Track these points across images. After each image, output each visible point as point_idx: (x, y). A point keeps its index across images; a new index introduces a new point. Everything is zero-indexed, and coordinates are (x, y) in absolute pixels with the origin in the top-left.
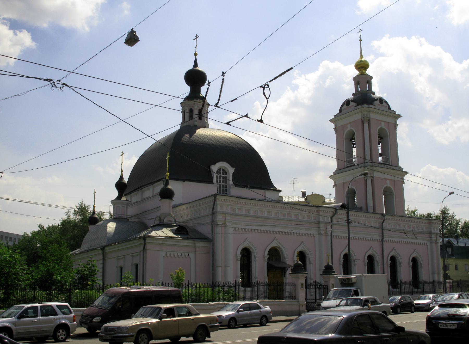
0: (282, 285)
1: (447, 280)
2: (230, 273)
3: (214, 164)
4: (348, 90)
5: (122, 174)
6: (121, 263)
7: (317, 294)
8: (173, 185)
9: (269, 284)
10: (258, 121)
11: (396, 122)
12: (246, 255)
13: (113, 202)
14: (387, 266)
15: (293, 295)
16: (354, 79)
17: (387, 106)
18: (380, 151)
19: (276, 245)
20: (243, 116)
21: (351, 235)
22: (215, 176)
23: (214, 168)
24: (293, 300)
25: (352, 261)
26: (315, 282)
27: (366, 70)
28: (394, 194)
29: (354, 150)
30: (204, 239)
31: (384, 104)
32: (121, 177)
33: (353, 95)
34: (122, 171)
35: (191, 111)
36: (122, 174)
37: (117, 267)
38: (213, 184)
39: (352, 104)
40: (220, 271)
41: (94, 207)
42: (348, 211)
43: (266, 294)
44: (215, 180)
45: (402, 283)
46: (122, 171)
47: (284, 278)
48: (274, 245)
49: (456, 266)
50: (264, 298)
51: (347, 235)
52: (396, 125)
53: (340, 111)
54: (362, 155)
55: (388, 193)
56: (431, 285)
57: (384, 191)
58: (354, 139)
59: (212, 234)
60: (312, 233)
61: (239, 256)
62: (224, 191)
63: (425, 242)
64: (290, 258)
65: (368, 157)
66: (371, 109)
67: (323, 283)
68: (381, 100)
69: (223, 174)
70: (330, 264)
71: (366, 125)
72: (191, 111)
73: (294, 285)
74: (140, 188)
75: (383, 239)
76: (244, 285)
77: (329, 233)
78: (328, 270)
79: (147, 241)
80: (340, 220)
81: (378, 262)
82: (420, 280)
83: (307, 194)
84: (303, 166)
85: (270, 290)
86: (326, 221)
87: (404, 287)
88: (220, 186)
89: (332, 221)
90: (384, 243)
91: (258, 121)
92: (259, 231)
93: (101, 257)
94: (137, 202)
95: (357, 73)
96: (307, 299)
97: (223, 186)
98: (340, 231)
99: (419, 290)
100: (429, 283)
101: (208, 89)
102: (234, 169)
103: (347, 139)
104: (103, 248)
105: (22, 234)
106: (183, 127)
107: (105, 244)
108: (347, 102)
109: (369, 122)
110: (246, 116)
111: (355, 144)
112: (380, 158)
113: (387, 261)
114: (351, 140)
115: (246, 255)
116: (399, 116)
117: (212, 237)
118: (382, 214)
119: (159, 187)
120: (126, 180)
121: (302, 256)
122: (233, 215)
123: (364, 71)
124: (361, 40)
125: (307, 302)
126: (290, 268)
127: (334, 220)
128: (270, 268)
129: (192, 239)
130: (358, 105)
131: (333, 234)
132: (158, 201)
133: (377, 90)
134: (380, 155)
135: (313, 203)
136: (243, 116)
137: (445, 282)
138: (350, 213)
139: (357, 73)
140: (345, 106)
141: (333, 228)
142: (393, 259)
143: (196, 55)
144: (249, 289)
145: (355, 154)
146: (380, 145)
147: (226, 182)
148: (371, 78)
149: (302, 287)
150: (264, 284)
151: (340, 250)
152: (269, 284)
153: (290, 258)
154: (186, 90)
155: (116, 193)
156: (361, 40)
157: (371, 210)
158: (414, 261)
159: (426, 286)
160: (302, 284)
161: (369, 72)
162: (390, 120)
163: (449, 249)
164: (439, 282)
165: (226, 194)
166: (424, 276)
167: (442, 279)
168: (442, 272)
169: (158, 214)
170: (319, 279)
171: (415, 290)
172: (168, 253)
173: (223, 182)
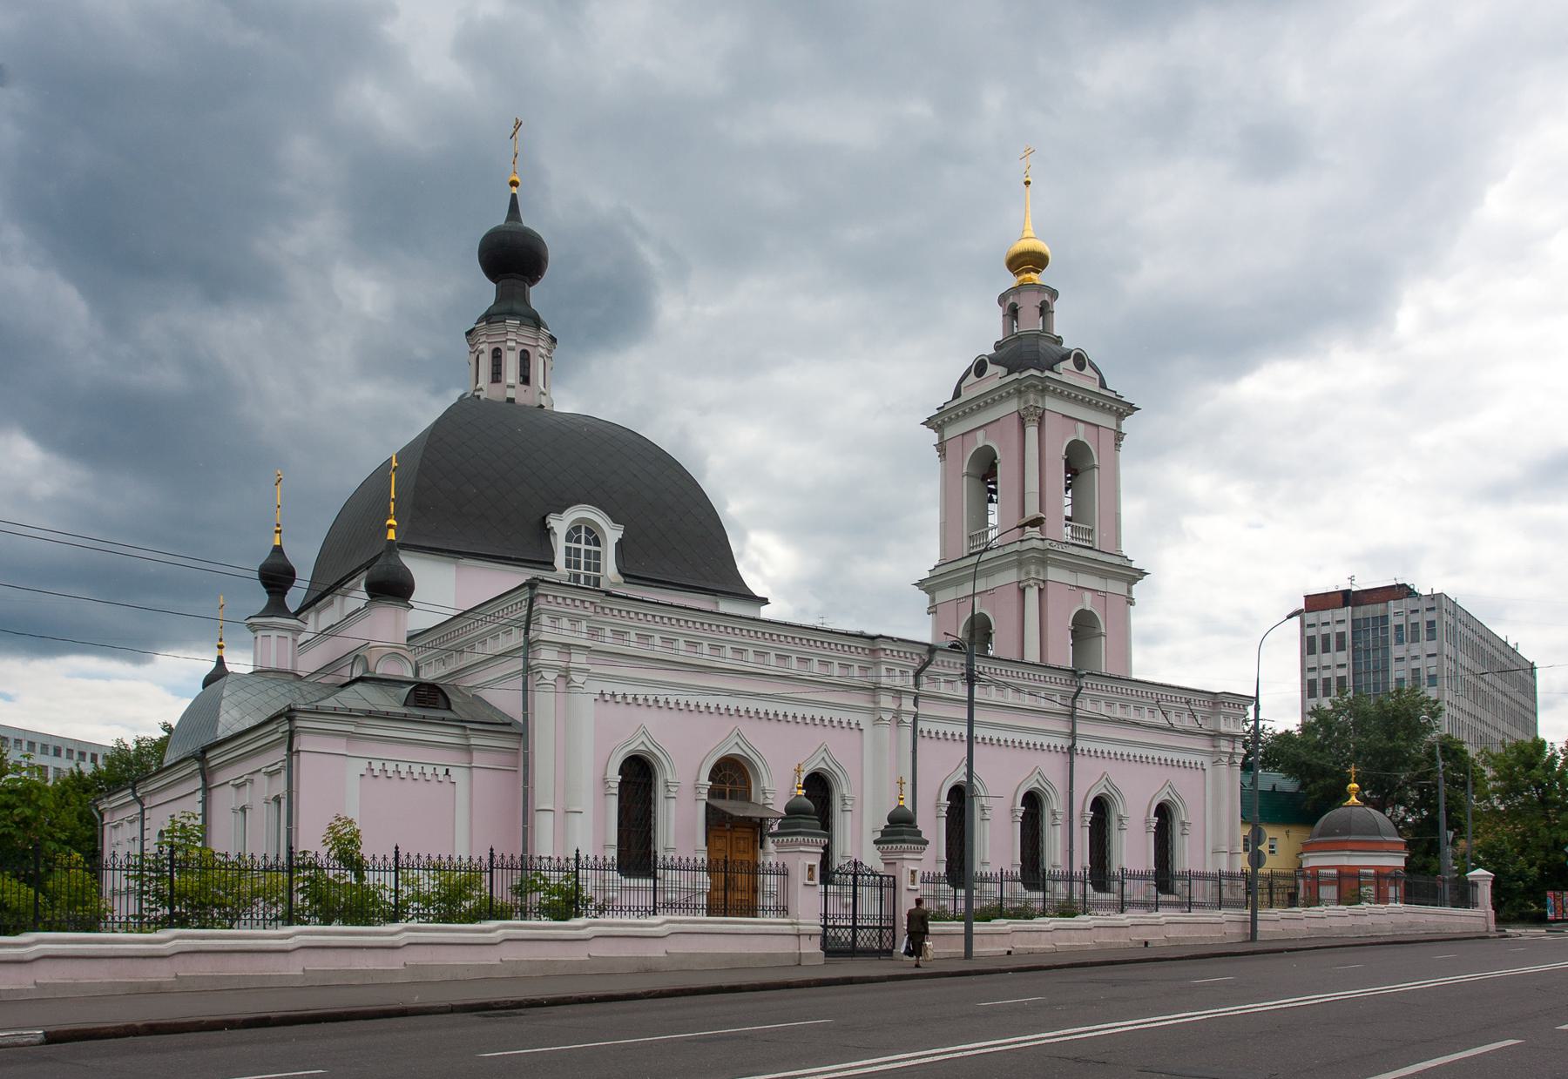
2: (582, 828)
4: (988, 330)
7: (14, 969)
9: (711, 869)
12: (638, 777)
18: (1068, 512)
22: (560, 545)
23: (559, 525)
31: (1088, 371)
39: (991, 369)
40: (545, 827)
43: (703, 900)
45: (1126, 875)
50: (687, 907)
53: (957, 394)
61: (615, 778)
63: (1199, 759)
64: (777, 789)
67: (880, 867)
69: (588, 543)
70: (909, 807)
71: (1032, 431)
73: (784, 873)
77: (909, 719)
78: (900, 828)
79: (298, 723)
82: (1115, 869)
85: (714, 888)
86: (898, 682)
87: (1130, 886)
93: (198, 783)
97: (587, 578)
98: (945, 718)
99: (1171, 898)
105: (113, 744)
115: (638, 777)
116: (1132, 408)
121: (819, 786)
125: (825, 927)
128: (716, 822)
129: (460, 723)
133: (1069, 326)
140: (972, 378)
142: (1101, 806)
145: (993, 519)
147: (597, 568)
148: (1054, 294)
149: (811, 879)
151: (941, 769)
153: (777, 789)
158: (1164, 812)
160: (811, 868)
166: (1187, 857)
170: (872, 858)
172: (377, 766)
173: (587, 568)
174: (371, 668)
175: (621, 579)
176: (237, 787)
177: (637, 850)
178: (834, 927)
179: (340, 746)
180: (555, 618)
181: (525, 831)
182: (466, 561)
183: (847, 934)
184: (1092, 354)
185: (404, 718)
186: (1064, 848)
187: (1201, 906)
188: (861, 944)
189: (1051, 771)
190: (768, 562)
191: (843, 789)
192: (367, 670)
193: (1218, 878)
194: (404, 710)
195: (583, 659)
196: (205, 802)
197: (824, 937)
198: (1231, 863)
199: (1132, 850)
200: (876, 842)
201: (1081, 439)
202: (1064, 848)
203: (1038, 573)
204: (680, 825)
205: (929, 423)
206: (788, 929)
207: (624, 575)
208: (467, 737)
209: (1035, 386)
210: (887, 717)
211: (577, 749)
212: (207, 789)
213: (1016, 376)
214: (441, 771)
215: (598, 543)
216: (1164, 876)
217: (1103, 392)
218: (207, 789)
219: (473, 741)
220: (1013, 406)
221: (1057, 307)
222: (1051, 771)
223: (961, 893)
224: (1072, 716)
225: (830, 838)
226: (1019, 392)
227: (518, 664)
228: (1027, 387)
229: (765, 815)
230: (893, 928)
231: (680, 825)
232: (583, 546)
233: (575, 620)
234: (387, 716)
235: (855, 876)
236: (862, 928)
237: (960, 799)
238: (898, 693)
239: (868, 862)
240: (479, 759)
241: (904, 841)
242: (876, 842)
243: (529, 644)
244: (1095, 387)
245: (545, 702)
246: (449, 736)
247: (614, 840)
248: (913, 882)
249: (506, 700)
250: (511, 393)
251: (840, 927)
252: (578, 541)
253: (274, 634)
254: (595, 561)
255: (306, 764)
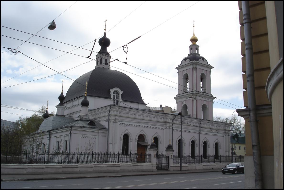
0: (145, 155)
1: (233, 155)
2: (118, 148)
3: (112, 89)
4: (186, 53)
5: (62, 92)
6: (59, 140)
8: (89, 99)
10: (124, 63)
11: (210, 70)
12: (126, 138)
13: (57, 107)
14: (202, 147)
15: (150, 160)
16: (190, 47)
17: (206, 62)
18: (201, 86)
19: (142, 133)
20: (116, 60)
21: (182, 129)
22: (112, 94)
23: (112, 91)
24: (150, 164)
25: (183, 144)
26: (162, 154)
27: (196, 42)
28: (207, 109)
29: (188, 84)
30: (104, 129)
31: (205, 61)
32: (62, 94)
33: (189, 55)
34: (62, 90)
35: (101, 60)
36: (62, 92)
37: (56, 142)
38: (111, 99)
39: (187, 60)
40: (111, 146)
41: (47, 109)
42: (182, 117)
43: (136, 160)
44: (112, 97)
46: (62, 90)
47: (146, 151)
48: (141, 133)
49: (240, 147)
50: (134, 161)
51: (180, 129)
52: (210, 72)
53: (181, 63)
54: (192, 88)
55: (204, 107)
56: (225, 158)
57: (202, 107)
58: (188, 79)
59: (108, 126)
60: (162, 127)
62: (116, 103)
64: (149, 141)
65: (195, 89)
66: (197, 63)
68: (203, 59)
70: (171, 144)
72: (101, 60)
74: (71, 100)
75: (200, 132)
76: (123, 154)
77: (171, 128)
78: (170, 148)
79: (72, 129)
80: (177, 121)
81: (197, 144)
82: (219, 155)
83: (163, 106)
84: (160, 91)
87: (210, 158)
88: (114, 100)
89: (173, 122)
90: (201, 135)
91: (124, 63)
92: (135, 126)
93: (48, 136)
94: (70, 107)
95: (191, 43)
96: (157, 163)
98: (177, 127)
99: (218, 160)
100: (224, 156)
101: (95, 43)
102: (123, 91)
103: (184, 78)
104: (49, 131)
106: (96, 68)
107: (51, 129)
108: (185, 59)
109: (196, 70)
110: (117, 59)
111: (188, 81)
112: (201, 89)
113: (202, 144)
114: (186, 79)
115: (126, 138)
116: (212, 67)
117: (108, 128)
118: (200, 120)
119: (81, 100)
120: (65, 95)
121: (156, 140)
122: (120, 116)
123: (195, 43)
124: (194, 26)
125: (157, 165)
126: (150, 146)
127: (174, 121)
128: (139, 146)
129: (97, 128)
130: (191, 61)
131: (173, 129)
132: (80, 108)
133: (202, 53)
134: (201, 87)
135: (163, 112)
136: (116, 60)
137: (232, 157)
138: (183, 118)
139: (191, 43)
140: (184, 61)
141: (173, 125)
143: (105, 30)
144: (127, 156)
145: (188, 86)
146: (202, 82)
147: (118, 98)
148: (199, 46)
149: (155, 157)
150: (135, 154)
152: (138, 154)
153: (149, 141)
154: (98, 48)
155: (58, 102)
156: (194, 26)
157: (195, 117)
158: (217, 144)
159: (222, 158)
160: (155, 155)
161: (197, 43)
162: (208, 69)
163: (236, 139)
164: (229, 156)
165: (118, 105)
166: (221, 153)
167: (231, 155)
168: (231, 151)
169: (80, 114)
170: (165, 153)
171: (216, 160)
174: (82, 117)
175: (122, 101)
176: (57, 138)
177: (125, 150)
178: (158, 165)
179: (78, 132)
180: (114, 111)
181: (107, 147)
182: (96, 98)
183: (161, 166)
184: (205, 57)
185: (89, 127)
186: (199, 151)
187: (223, 162)
188: (163, 168)
189: (196, 136)
190: (146, 97)
191: (160, 140)
192: (81, 118)
193: (226, 156)
194: (88, 126)
195: (118, 118)
196: (49, 140)
197: (157, 167)
198: (229, 154)
199: (211, 152)
200: (165, 150)
201: (203, 73)
202: (199, 151)
203: (196, 97)
204: (133, 147)
205: (176, 68)
206: (151, 165)
207: (123, 100)
208: (98, 131)
209: (195, 64)
210: (168, 127)
211: (117, 133)
212: (50, 137)
213: (191, 62)
214: (94, 136)
215: (118, 94)
216: (217, 156)
217: (207, 64)
218: (50, 137)
219: (99, 131)
220: (191, 67)
221: (199, 48)
222: (196, 136)
223: (180, 159)
224: (200, 127)
225: (158, 149)
226: (192, 64)
227: (107, 118)
228: (194, 64)
229: (147, 145)
230: (168, 165)
231: (133, 147)
232: (116, 95)
233: (117, 111)
234: (86, 127)
235: (162, 156)
236: (163, 165)
237: (180, 142)
238: (170, 123)
239: (164, 154)
240: (100, 134)
241: (170, 150)
242: (165, 150)
243: (109, 115)
244: (206, 64)
245: (111, 124)
246: (95, 130)
247: (122, 148)
248: (172, 157)
249: (105, 124)
250: (103, 67)
251: (159, 165)
252: (115, 94)
253: (61, 109)
254: (118, 98)
255: (73, 135)
